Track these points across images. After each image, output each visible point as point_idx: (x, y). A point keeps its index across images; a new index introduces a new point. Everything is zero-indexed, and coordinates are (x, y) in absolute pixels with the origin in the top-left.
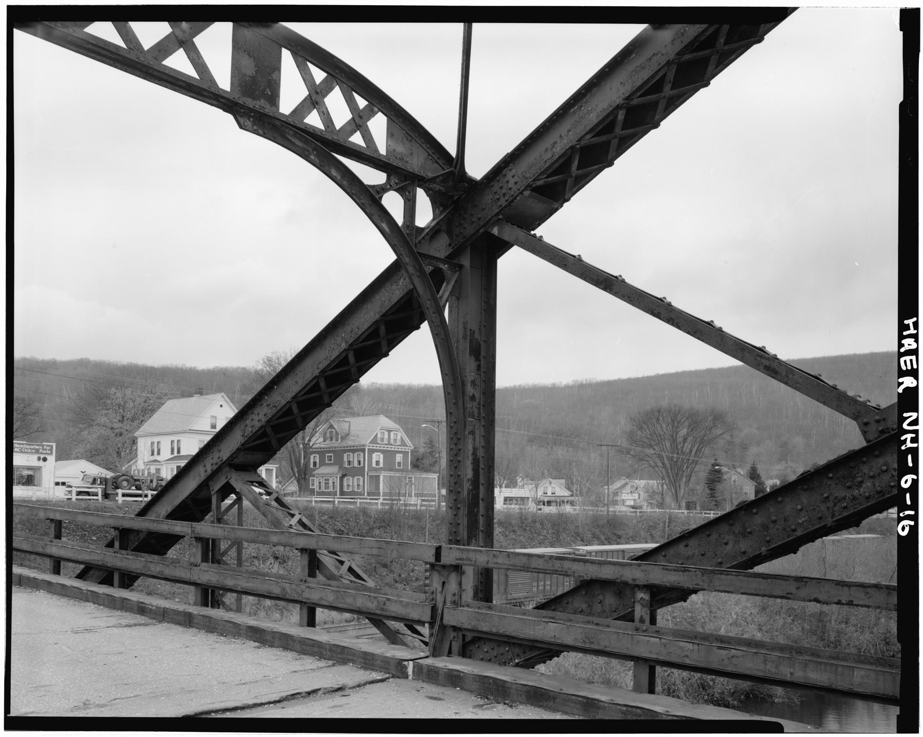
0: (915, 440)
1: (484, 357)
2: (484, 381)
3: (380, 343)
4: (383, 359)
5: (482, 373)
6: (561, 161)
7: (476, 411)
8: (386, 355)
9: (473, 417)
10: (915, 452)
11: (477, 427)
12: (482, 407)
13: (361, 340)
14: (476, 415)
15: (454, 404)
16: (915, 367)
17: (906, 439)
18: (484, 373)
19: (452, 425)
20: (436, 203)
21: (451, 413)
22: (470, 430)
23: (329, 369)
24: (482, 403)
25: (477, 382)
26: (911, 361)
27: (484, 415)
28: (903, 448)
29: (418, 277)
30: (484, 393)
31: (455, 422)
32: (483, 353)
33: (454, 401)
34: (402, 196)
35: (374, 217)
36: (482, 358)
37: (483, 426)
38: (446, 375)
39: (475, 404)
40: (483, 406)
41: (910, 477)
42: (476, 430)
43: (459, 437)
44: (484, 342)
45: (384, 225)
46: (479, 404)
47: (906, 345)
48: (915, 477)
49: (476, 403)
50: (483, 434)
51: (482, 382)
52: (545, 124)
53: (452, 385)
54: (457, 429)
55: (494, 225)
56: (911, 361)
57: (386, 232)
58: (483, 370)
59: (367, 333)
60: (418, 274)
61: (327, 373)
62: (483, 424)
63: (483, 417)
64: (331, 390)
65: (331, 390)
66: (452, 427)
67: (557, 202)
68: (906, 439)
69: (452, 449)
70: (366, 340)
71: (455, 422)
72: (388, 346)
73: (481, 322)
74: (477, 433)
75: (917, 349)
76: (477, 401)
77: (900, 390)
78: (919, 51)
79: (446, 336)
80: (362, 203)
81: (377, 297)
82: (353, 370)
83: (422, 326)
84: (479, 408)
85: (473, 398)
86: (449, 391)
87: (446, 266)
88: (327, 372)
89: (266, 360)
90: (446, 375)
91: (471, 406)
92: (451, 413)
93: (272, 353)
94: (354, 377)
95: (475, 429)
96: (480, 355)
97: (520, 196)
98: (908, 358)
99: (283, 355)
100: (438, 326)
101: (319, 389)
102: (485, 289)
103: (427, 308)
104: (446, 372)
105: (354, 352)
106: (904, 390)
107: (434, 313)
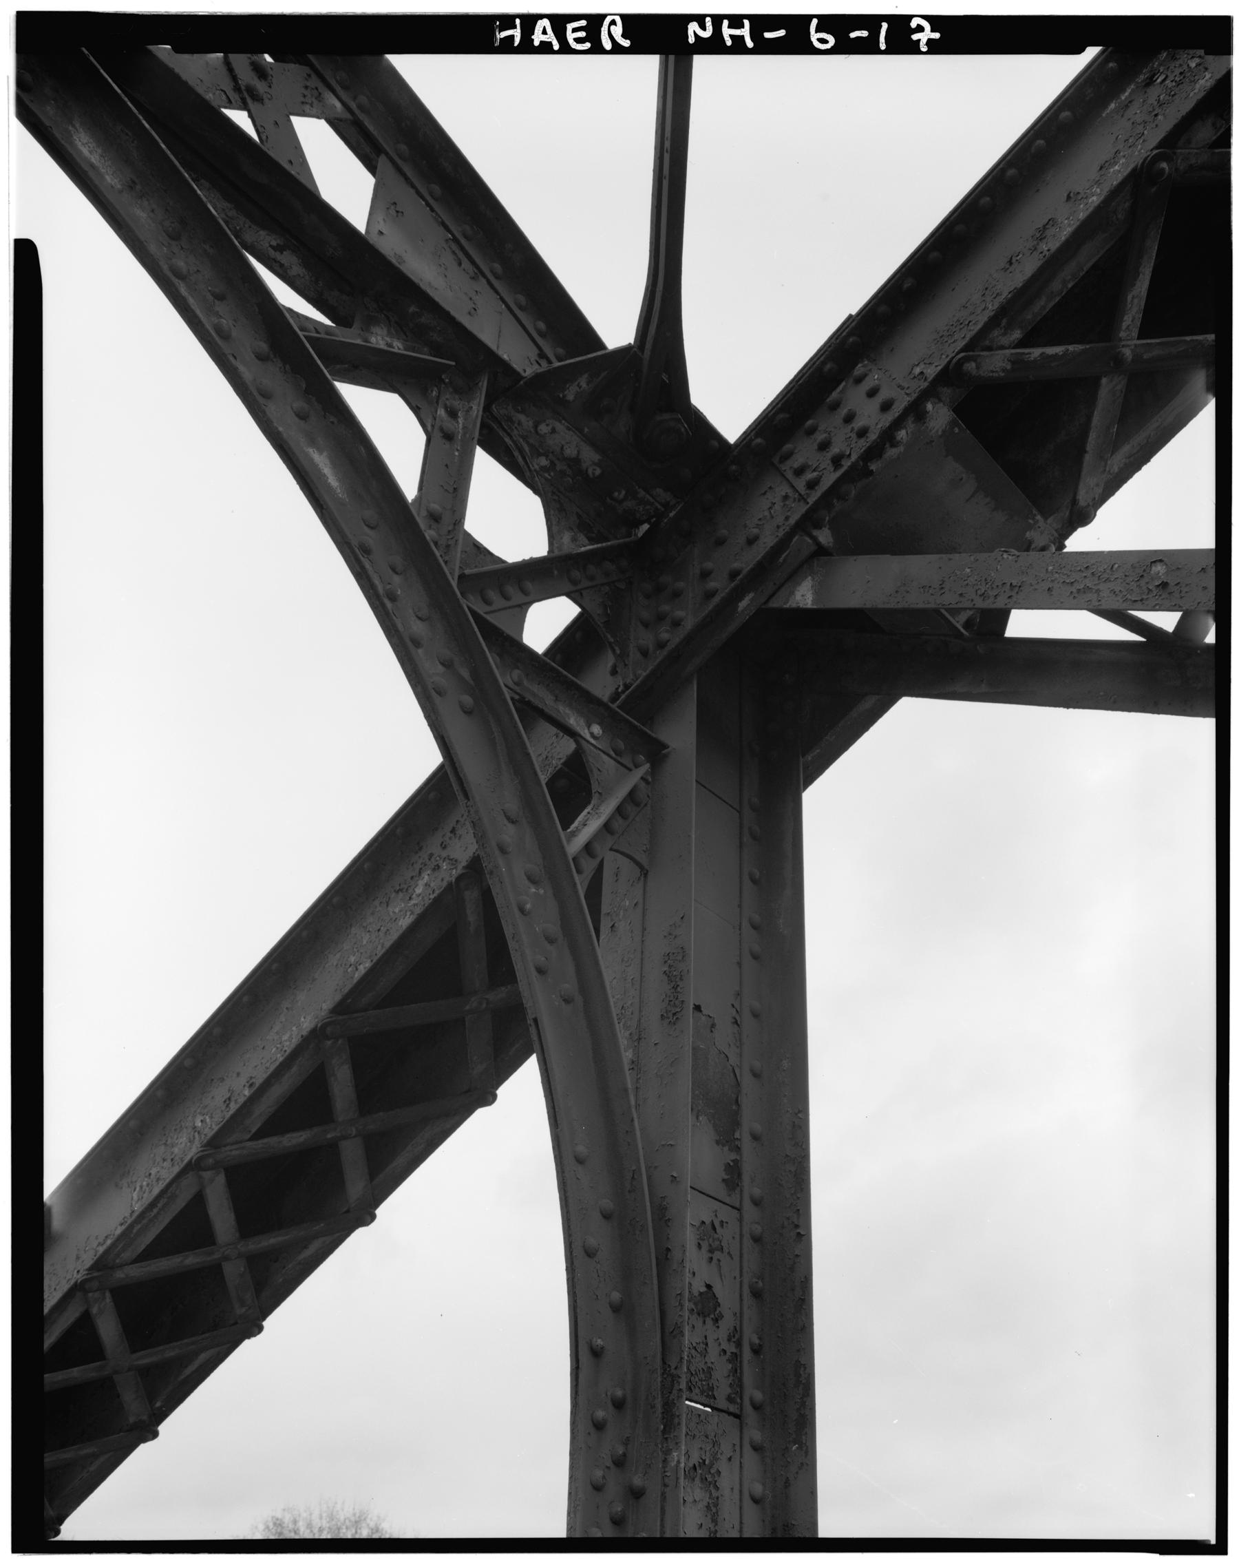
0: (736, 21)
1: (755, 1137)
2: (757, 1239)
3: (333, 1147)
4: (360, 1229)
5: (748, 1206)
6: (1088, 257)
7: (721, 1370)
8: (365, 1216)
9: (708, 1396)
10: (761, 23)
11: (726, 1449)
12: (747, 1354)
13: (255, 1122)
14: (723, 1391)
15: (616, 1309)
16: (583, 23)
17: (731, 36)
18: (756, 1203)
19: (600, 1414)
20: (562, 509)
21: (596, 1353)
22: (695, 1459)
23: (128, 1255)
24: (750, 1336)
25: (727, 1235)
26: (575, 30)
27: (758, 1396)
28: (750, 44)
29: (468, 712)
30: (757, 1294)
31: (619, 1405)
32: (750, 1121)
33: (616, 1296)
34: (416, 410)
35: (272, 409)
36: (744, 1135)
37: (756, 1448)
38: (580, 1161)
39: (718, 1335)
40: (756, 1351)
41: (814, 37)
42: (723, 1465)
43: (637, 1481)
44: (756, 1075)
45: (321, 461)
46: (735, 1336)
47: (544, 38)
48: (815, 22)
49: (723, 1333)
50: (758, 1489)
51: (748, 1242)
52: (1003, 171)
53: (607, 1216)
54: (626, 1442)
55: (793, 577)
56: (575, 30)
57: (329, 486)
58: (751, 1187)
59: (279, 1091)
60: (468, 700)
61: (119, 1275)
62: (757, 1435)
63: (756, 1407)
64: (146, 1358)
65: (146, 1358)
66: (599, 1426)
67: (1046, 516)
68: (731, 36)
69: (598, 1488)
70: (273, 1126)
71: (619, 1405)
72: (372, 1175)
73: (738, 994)
74: (728, 1480)
75: (551, 17)
76: (727, 1323)
77: (626, 43)
78: (1161, 1554)
79: (583, 989)
80: (219, 330)
81: (333, 959)
82: (233, 1271)
83: (504, 1091)
84: (735, 1358)
85: (707, 1304)
86: (592, 1242)
87: (596, 729)
88: (121, 1266)
89: (271, 1525)
90: (580, 1161)
91: (697, 1339)
92: (596, 1353)
93: (284, 1510)
94: (240, 1311)
95: (715, 1458)
96: (736, 1123)
97: (910, 424)
98: (571, 37)
99: (304, 1515)
100: (551, 941)
101: (96, 1352)
102: (754, 881)
103: (503, 850)
104: (581, 1149)
105: (230, 1183)
106: (881, 26)
107: (532, 880)
